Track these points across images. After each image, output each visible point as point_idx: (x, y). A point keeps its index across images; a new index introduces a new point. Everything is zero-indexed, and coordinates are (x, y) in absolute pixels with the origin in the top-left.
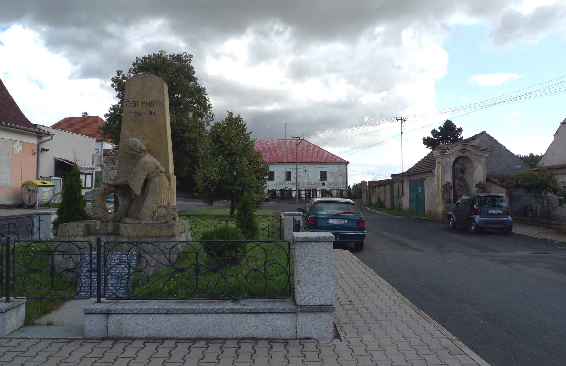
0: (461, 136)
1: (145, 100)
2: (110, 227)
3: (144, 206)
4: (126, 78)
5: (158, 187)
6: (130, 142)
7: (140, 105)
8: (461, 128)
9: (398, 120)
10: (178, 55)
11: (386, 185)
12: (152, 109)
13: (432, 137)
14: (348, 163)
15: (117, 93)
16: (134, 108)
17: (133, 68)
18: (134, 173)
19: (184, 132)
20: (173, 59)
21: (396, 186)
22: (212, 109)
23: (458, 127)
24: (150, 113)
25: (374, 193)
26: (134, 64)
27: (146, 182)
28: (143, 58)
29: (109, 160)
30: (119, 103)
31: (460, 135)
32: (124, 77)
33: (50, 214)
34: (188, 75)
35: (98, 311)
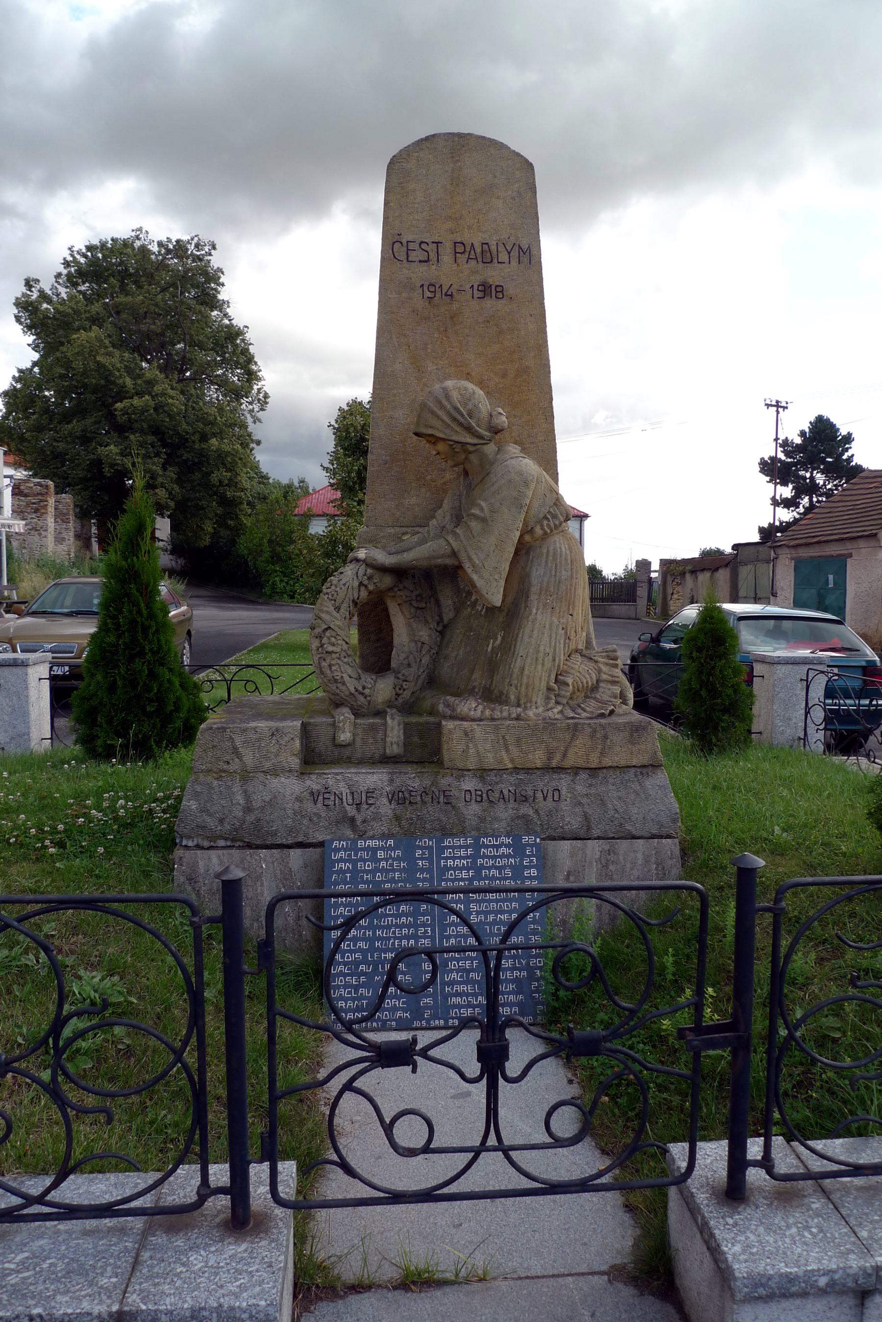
0: (849, 453)
1: (467, 237)
2: (394, 732)
3: (521, 650)
4: (49, 301)
5: (564, 574)
6: (455, 395)
7: (447, 258)
8: (850, 434)
9: (768, 406)
10: (178, 241)
11: (717, 569)
12: (494, 275)
13: (781, 456)
14: (586, 516)
15: (31, 339)
16: (423, 268)
17: (65, 272)
18: (483, 520)
19: (204, 438)
20: (168, 251)
21: (745, 572)
22: (263, 383)
23: (843, 432)
24: (486, 290)
25: (679, 588)
26: (66, 264)
27: (523, 550)
28: (89, 248)
29: (28, 505)
30: (35, 364)
31: (847, 450)
32: (43, 296)
33: (24, 664)
34: (208, 294)
35: (823, 1281)
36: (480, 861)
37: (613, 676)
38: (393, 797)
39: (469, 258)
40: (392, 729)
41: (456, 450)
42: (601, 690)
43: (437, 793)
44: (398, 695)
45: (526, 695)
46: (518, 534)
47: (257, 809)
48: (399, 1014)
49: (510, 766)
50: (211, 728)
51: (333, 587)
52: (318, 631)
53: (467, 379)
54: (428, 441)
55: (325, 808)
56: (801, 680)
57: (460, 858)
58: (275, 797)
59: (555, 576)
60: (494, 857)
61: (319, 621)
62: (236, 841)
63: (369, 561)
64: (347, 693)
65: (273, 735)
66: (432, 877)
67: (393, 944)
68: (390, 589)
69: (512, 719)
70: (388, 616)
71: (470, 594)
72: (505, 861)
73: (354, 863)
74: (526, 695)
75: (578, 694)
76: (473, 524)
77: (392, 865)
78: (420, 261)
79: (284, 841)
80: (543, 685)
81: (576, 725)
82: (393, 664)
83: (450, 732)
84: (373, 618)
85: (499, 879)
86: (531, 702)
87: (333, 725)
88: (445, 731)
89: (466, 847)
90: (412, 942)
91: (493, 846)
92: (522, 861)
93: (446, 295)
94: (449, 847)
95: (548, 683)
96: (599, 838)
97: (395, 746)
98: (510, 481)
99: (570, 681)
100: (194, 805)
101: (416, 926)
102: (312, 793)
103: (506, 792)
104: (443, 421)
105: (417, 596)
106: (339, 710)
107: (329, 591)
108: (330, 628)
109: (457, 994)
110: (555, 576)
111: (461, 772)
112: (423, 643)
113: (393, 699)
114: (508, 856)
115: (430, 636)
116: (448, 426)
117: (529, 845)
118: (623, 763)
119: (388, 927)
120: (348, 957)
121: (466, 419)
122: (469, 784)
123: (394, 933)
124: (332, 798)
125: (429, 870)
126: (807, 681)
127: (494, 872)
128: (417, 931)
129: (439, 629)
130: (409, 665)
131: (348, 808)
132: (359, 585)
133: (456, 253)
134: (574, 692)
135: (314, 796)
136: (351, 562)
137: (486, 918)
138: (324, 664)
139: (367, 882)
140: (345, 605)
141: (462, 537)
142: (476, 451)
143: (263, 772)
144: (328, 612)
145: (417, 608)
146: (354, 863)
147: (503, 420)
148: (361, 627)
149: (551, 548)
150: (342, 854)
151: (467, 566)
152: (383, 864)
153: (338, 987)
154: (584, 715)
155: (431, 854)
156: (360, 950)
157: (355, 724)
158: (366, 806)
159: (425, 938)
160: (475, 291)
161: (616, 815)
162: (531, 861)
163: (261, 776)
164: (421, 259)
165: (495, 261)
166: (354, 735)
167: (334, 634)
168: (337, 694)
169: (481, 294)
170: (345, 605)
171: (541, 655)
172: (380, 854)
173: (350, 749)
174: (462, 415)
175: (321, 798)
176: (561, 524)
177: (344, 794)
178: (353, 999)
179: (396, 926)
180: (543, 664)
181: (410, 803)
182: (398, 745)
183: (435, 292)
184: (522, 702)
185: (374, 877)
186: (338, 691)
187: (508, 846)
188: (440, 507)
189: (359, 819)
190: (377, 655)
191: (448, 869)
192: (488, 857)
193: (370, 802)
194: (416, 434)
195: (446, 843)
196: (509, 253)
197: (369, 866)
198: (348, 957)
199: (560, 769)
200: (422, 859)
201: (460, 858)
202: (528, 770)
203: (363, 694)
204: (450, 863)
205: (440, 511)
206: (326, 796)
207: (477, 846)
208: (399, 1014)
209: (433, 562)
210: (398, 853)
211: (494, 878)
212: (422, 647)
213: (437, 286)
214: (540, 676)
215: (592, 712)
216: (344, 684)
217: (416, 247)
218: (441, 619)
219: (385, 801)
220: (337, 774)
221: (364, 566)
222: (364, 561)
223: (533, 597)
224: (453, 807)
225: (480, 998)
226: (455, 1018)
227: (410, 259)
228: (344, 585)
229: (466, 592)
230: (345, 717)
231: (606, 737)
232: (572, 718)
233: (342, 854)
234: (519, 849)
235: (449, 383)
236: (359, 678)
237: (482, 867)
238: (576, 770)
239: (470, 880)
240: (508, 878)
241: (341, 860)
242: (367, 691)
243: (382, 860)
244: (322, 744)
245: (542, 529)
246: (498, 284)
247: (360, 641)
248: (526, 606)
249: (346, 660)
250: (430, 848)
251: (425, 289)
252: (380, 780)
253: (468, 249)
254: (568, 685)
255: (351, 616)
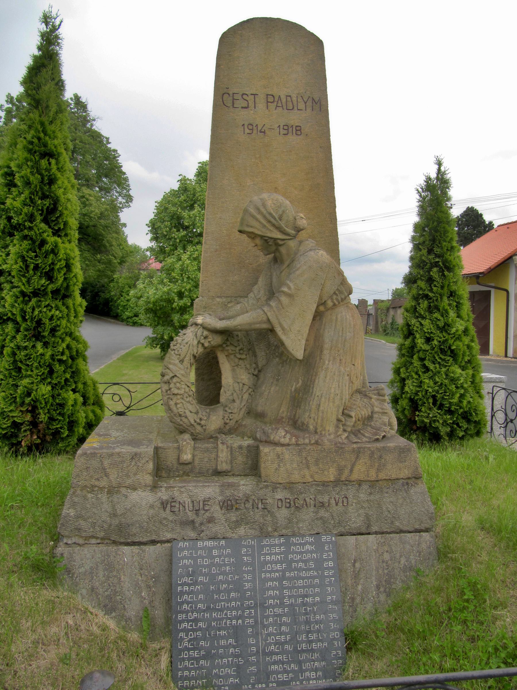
7: (261, 106)
16: (244, 112)
18: (290, 296)
36: (290, 556)
37: (382, 409)
38: (223, 504)
39: (277, 106)
40: (222, 450)
41: (270, 243)
42: (374, 419)
43: (256, 501)
44: (226, 424)
45: (322, 426)
46: (315, 306)
47: (121, 515)
48: (231, 680)
49: (311, 480)
50: (86, 454)
51: (178, 345)
52: (167, 378)
53: (276, 192)
54: (249, 237)
55: (172, 513)
56: (488, 393)
57: (276, 554)
58: (134, 506)
59: (342, 336)
60: (301, 553)
61: (167, 370)
62: (105, 539)
63: (206, 325)
64: (188, 424)
65: (132, 458)
66: (254, 569)
67: (226, 623)
68: (221, 346)
69: (312, 444)
70: (218, 362)
71: (277, 347)
72: (309, 556)
73: (195, 559)
74: (322, 426)
75: (359, 422)
76: (284, 299)
77: (224, 561)
78: (242, 108)
79: (141, 539)
80: (334, 418)
81: (359, 448)
82: (222, 399)
83: (266, 455)
84: (208, 368)
85: (306, 570)
86: (325, 430)
87: (178, 448)
88: (262, 454)
89: (280, 545)
90: (240, 621)
91: (300, 544)
92: (322, 555)
93: (261, 132)
94: (267, 546)
95: (337, 416)
96: (376, 533)
97: (224, 464)
98: (310, 267)
99: (353, 414)
100: (72, 512)
101: (242, 608)
102: (162, 503)
103: (308, 500)
104: (260, 222)
105: (240, 350)
106: (182, 436)
107: (175, 348)
108: (176, 376)
109: (275, 663)
110: (342, 336)
111: (275, 487)
112: (244, 384)
113: (222, 427)
114: (312, 552)
115: (249, 379)
116: (264, 226)
117: (327, 543)
118: (394, 476)
119: (221, 610)
120: (191, 635)
121: (277, 222)
122: (280, 495)
123: (226, 614)
124: (177, 506)
125: (252, 564)
126: (492, 394)
127: (301, 564)
128: (243, 612)
129: (256, 373)
130: (234, 401)
131: (190, 514)
132: (198, 343)
133: (268, 102)
134: (355, 422)
135: (164, 505)
136: (192, 325)
137: (296, 601)
138: (172, 403)
139: (205, 575)
140: (187, 358)
141: (275, 309)
142: (284, 244)
143: (125, 487)
144: (174, 365)
145: (240, 359)
146: (195, 559)
147: (303, 223)
148: (197, 369)
149: (339, 316)
150: (186, 553)
151: (278, 330)
152: (217, 560)
153: (183, 659)
154: (365, 439)
155: (253, 551)
156: (200, 629)
157: (195, 448)
158: (203, 512)
159: (250, 618)
160: (281, 130)
161: (389, 515)
162: (329, 555)
163: (123, 490)
164: (243, 106)
165: (296, 108)
166: (194, 456)
167: (179, 380)
168: (181, 425)
169: (285, 132)
170: (187, 358)
171: (332, 395)
172: (215, 552)
173: (190, 466)
174: (275, 219)
175: (169, 506)
176: (345, 298)
177: (187, 503)
178: (195, 669)
179: (228, 608)
180: (334, 402)
181: (236, 509)
182: (226, 463)
183: (252, 129)
184: (318, 431)
185: (210, 571)
186: (181, 423)
187: (310, 544)
188: (256, 283)
189: (198, 520)
190: (209, 389)
191: (266, 563)
192: (296, 553)
193: (206, 508)
194: (240, 231)
195: (265, 543)
196: (305, 103)
197: (206, 562)
198: (191, 635)
199: (348, 482)
200: (246, 555)
201: (276, 554)
202: (324, 484)
203: (200, 424)
204: (268, 558)
205: (256, 287)
206: (173, 504)
207: (288, 545)
208: (231, 680)
209: (253, 327)
210: (229, 551)
211: (300, 570)
212: (243, 387)
213: (254, 125)
214: (331, 410)
215: (370, 438)
216: (186, 417)
217: (240, 97)
218: (257, 366)
219: (218, 508)
220: (181, 487)
221: (201, 329)
222: (201, 325)
223: (326, 352)
224: (269, 511)
225: (292, 666)
226: (274, 682)
227: (235, 106)
228: (187, 343)
229: (278, 351)
230: (187, 443)
231: (381, 457)
232: (356, 443)
233: (186, 553)
234: (319, 547)
235: (265, 196)
236: (197, 413)
237: (292, 561)
238: (360, 483)
239: (284, 571)
240: (311, 569)
241: (185, 557)
242: (203, 422)
243: (216, 556)
244: (170, 458)
245: (333, 302)
246: (297, 124)
247: (197, 380)
248: (321, 359)
249: (188, 399)
250: (252, 547)
251: (246, 126)
252: (214, 491)
253: (276, 100)
254: (351, 417)
255: (191, 365)
